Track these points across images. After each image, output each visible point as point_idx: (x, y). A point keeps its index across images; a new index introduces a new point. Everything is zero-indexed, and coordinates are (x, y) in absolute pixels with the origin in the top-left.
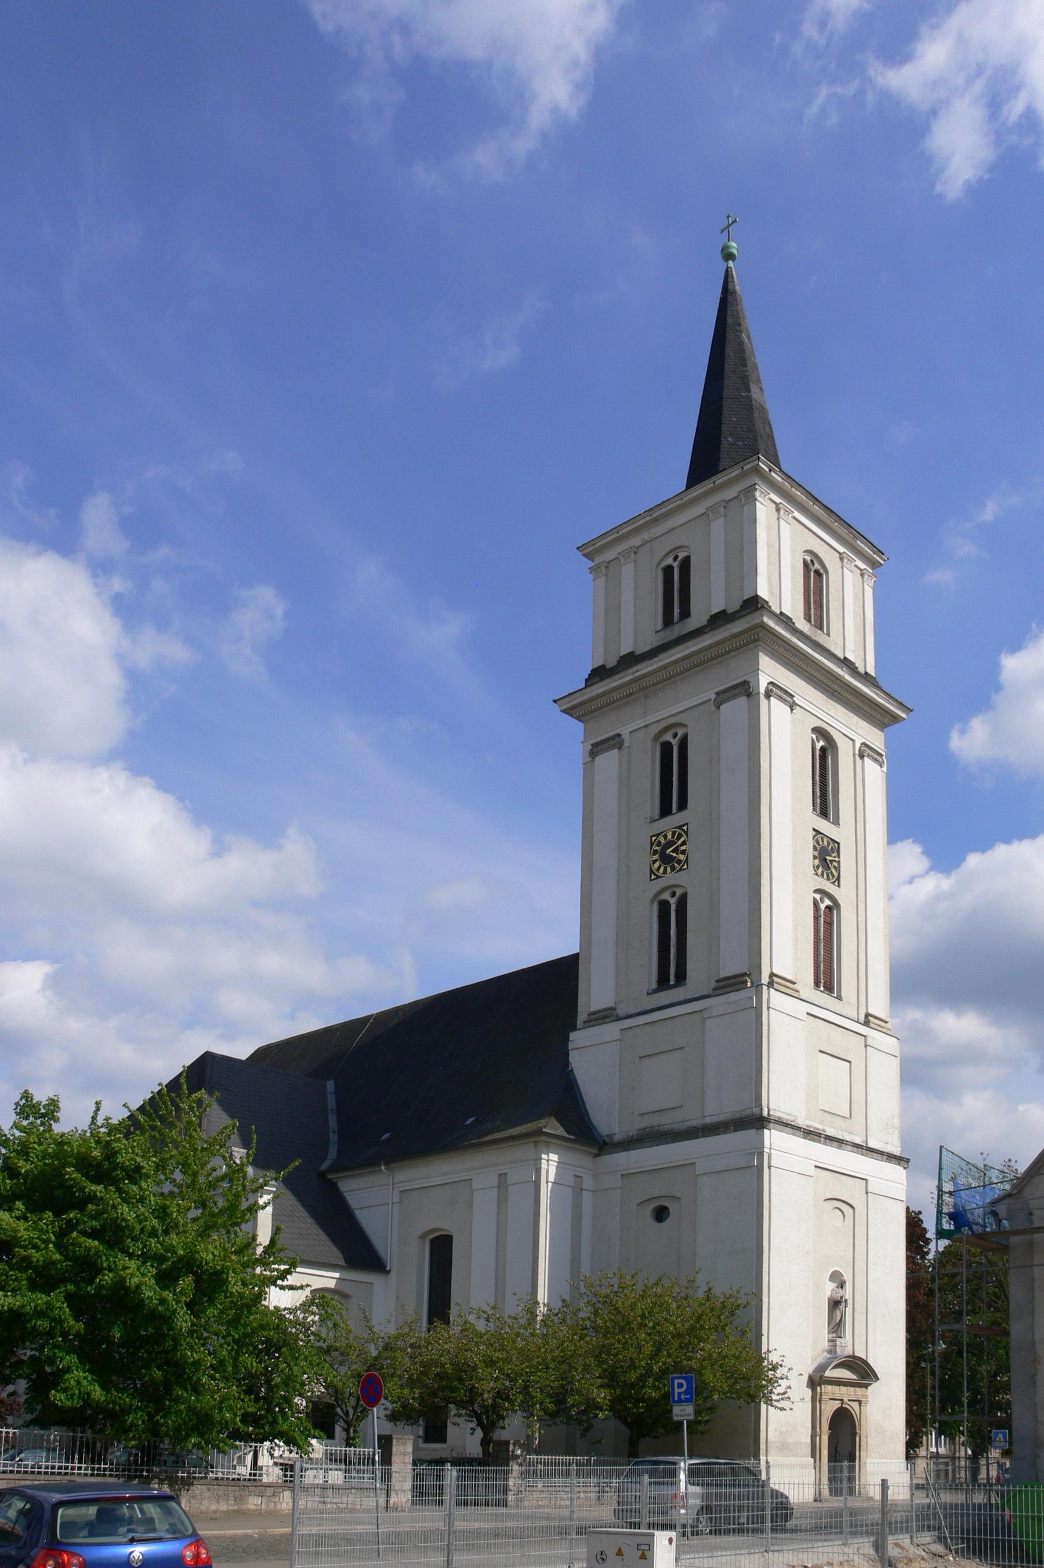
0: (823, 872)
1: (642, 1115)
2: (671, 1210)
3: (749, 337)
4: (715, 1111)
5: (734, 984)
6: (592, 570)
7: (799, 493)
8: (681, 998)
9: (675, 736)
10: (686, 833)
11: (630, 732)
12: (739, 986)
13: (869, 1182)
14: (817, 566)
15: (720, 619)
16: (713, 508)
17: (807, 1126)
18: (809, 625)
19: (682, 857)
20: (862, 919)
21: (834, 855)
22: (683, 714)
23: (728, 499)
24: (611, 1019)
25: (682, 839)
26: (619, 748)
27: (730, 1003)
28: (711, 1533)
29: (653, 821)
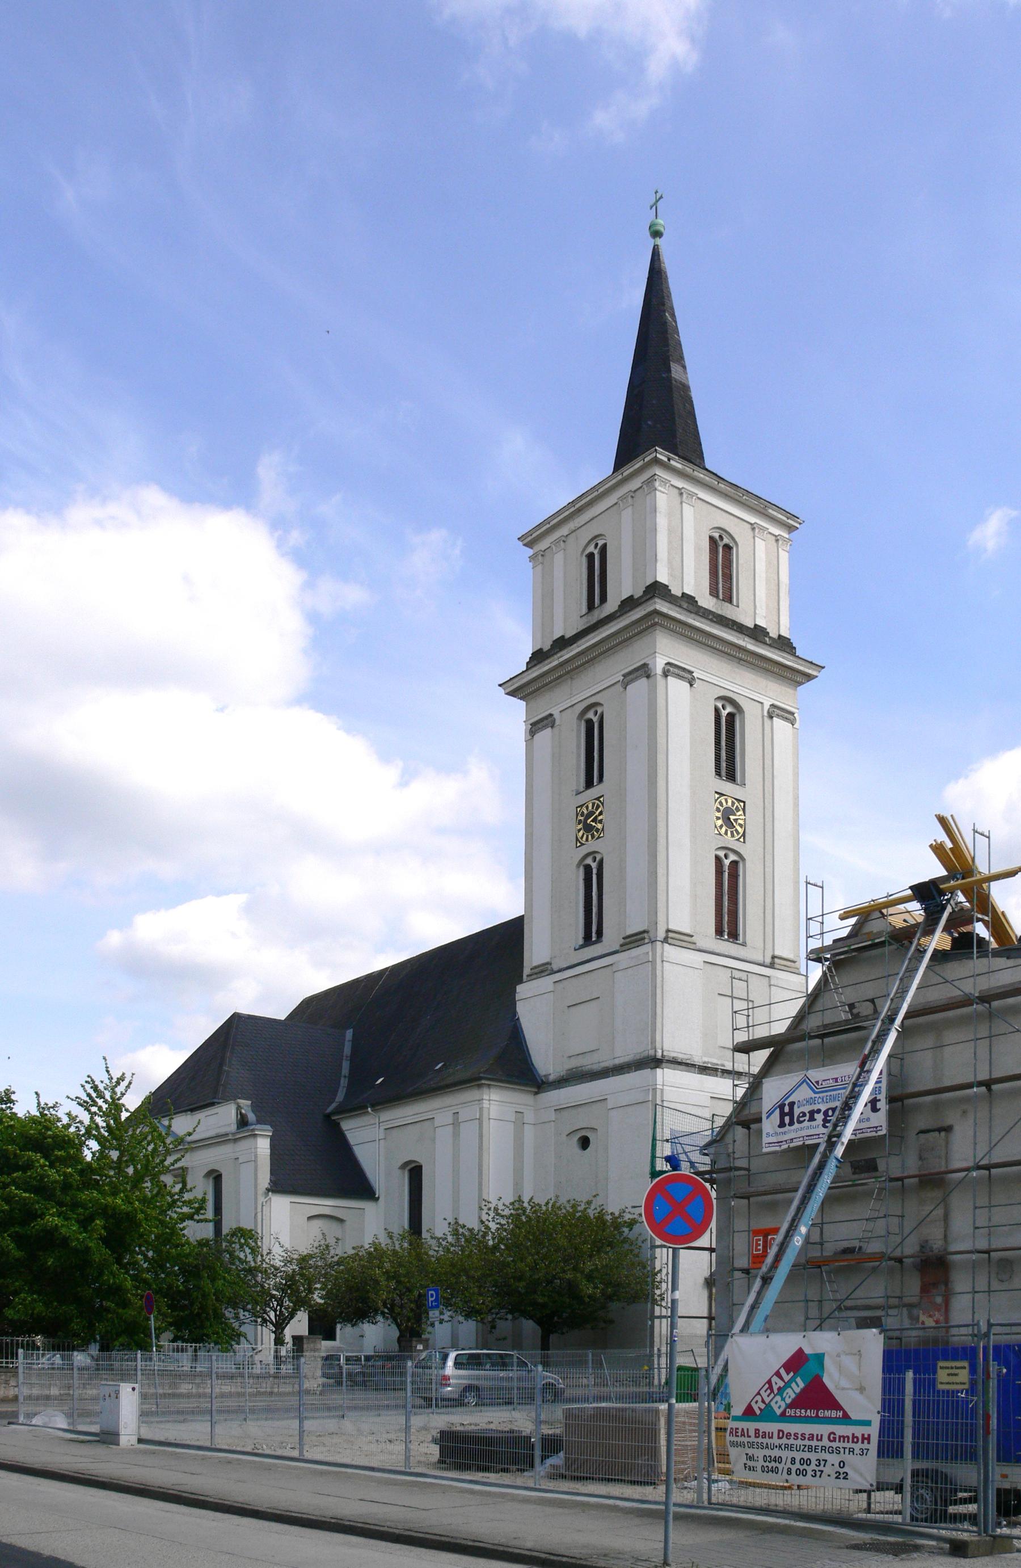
0: (726, 831)
1: (570, 1057)
2: (591, 1139)
3: (673, 315)
4: (624, 1053)
5: (636, 941)
6: (532, 558)
7: (702, 476)
12: (639, 943)
14: (726, 540)
15: (629, 604)
16: (622, 498)
17: (704, 1063)
18: (715, 599)
19: (599, 826)
20: (769, 870)
21: (738, 814)
22: (600, 694)
23: (635, 488)
24: (546, 973)
26: (552, 727)
27: (632, 958)
28: (476, 1405)
29: (578, 793)
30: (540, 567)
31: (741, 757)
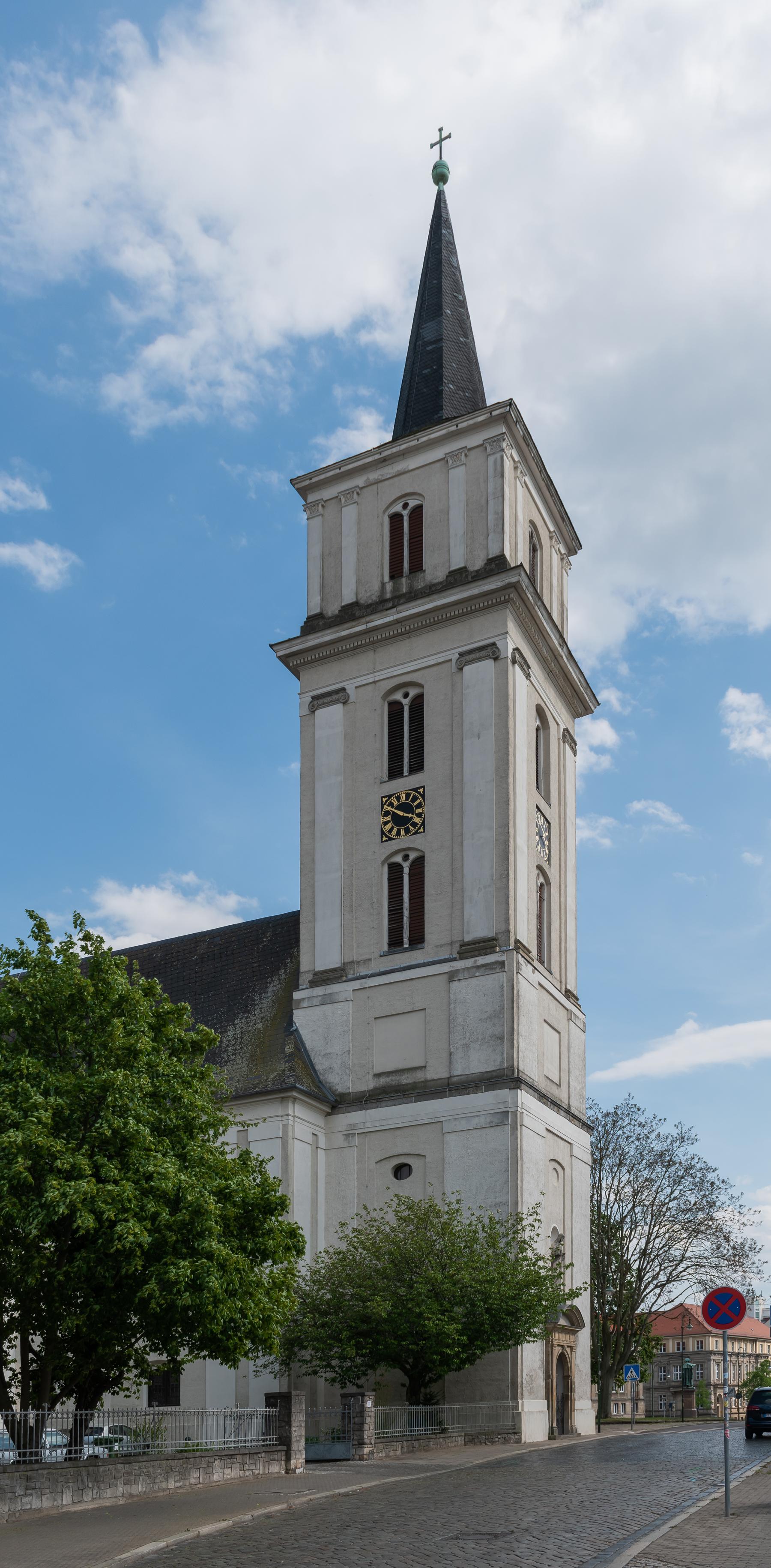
8: (420, 961)
9: (406, 695)
10: (423, 796)
11: (356, 687)
13: (574, 1147)
25: (418, 801)
26: (344, 703)
30: (318, 521)
31: (544, 777)
